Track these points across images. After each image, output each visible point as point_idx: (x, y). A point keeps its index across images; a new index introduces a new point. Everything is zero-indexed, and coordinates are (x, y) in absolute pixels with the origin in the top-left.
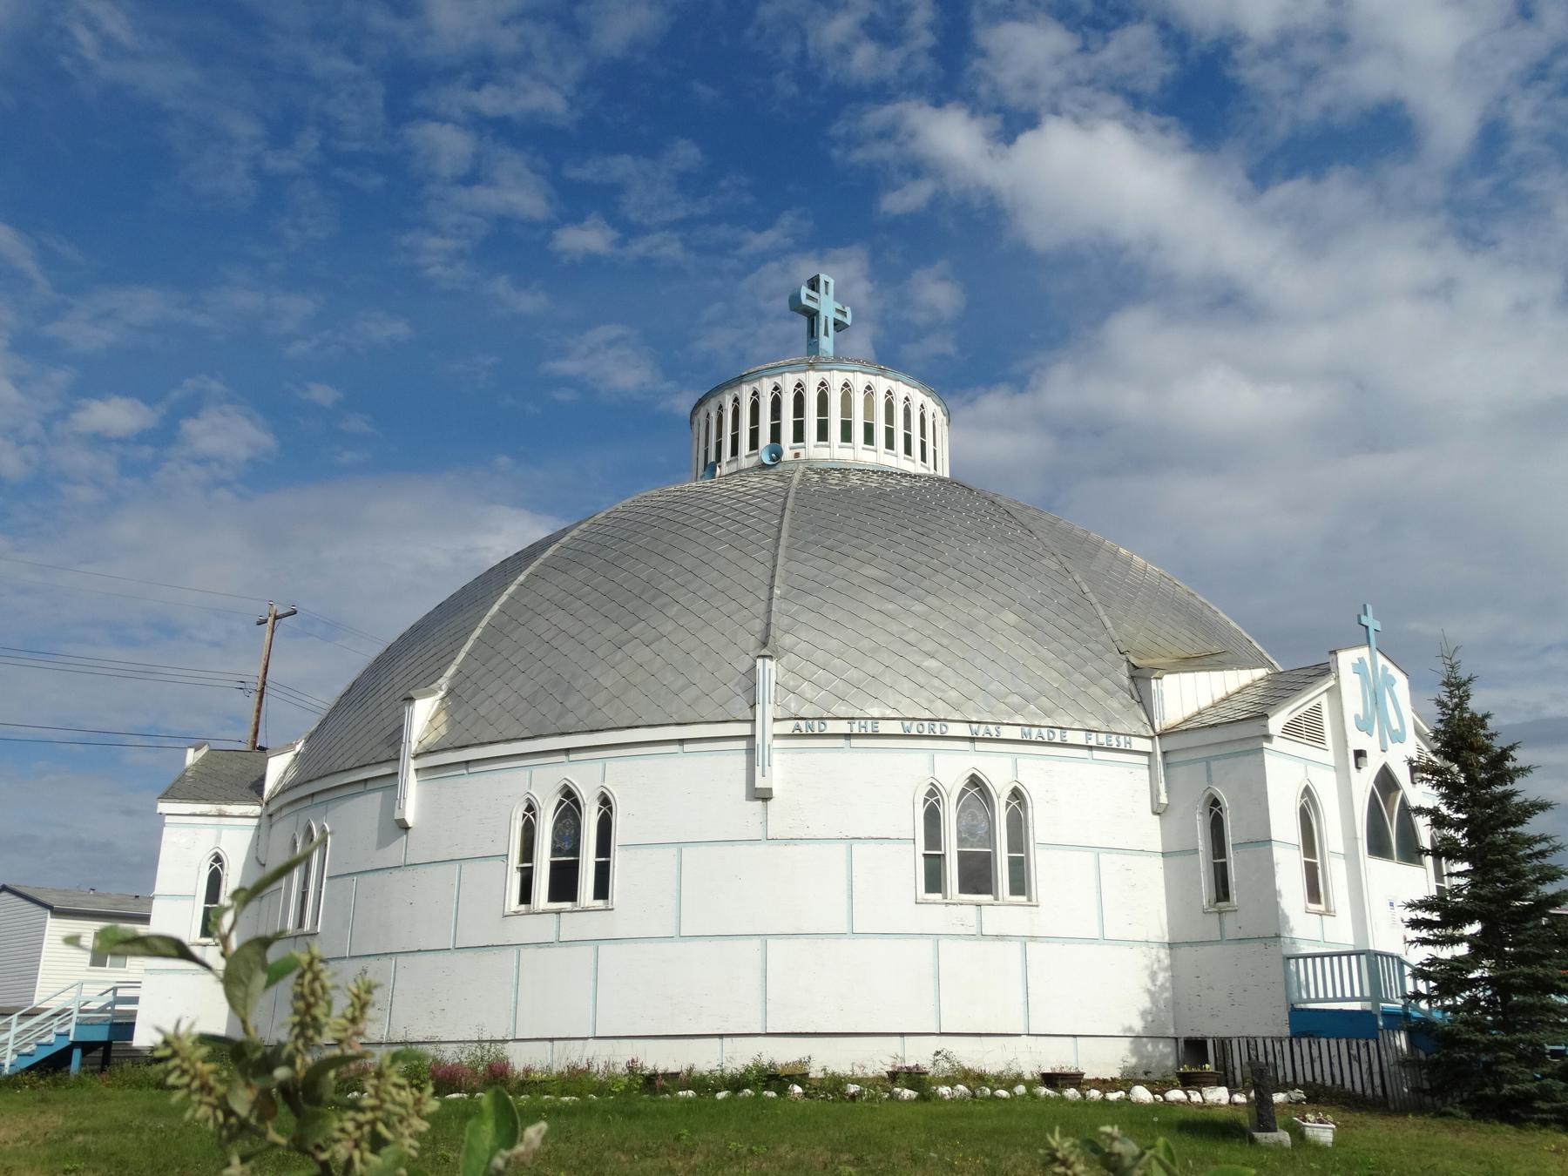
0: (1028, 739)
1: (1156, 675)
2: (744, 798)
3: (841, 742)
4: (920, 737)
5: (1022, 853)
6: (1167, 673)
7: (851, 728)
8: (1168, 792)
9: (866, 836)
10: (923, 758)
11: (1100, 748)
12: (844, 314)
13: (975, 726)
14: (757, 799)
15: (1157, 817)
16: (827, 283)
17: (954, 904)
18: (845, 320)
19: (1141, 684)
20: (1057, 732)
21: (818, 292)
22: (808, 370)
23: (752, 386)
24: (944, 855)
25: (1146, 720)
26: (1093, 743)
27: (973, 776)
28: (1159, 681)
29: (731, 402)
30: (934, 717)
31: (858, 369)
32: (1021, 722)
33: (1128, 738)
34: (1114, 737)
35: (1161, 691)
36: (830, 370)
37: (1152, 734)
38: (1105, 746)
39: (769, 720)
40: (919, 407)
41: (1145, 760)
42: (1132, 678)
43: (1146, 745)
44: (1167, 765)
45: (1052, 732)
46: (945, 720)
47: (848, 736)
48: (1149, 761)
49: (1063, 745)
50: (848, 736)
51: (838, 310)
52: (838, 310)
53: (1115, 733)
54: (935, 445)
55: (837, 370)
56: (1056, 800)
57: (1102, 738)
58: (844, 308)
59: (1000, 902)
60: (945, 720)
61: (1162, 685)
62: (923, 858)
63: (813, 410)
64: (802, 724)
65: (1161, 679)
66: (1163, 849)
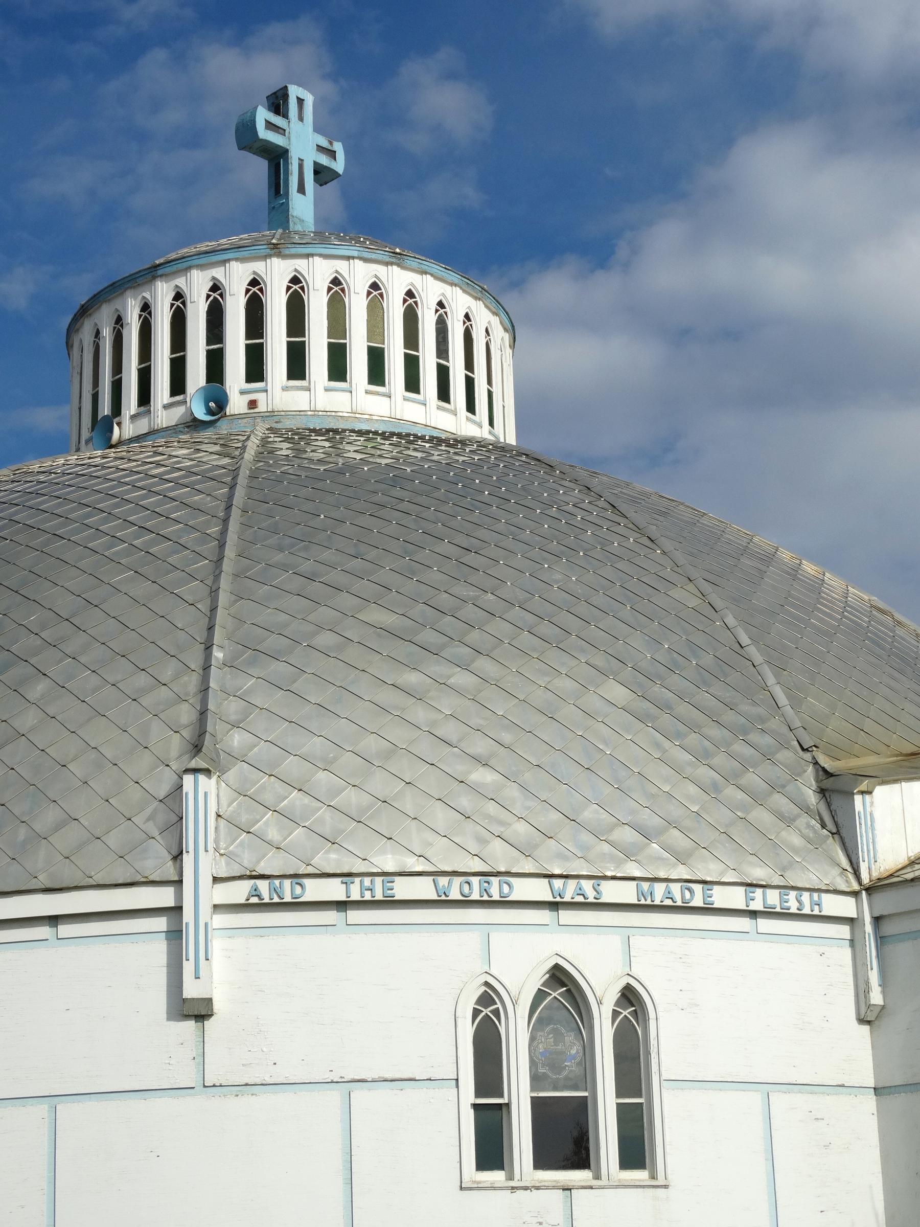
0: (649, 902)
3: (331, 916)
5: (640, 1096)
8: (883, 984)
9: (376, 1076)
10: (473, 938)
12: (332, 154)
13: (558, 883)
14: (187, 1017)
15: (866, 1029)
16: (300, 101)
17: (526, 1188)
19: (837, 801)
20: (697, 888)
24: (508, 1105)
28: (867, 797)
31: (355, 254)
32: (637, 873)
33: (815, 895)
34: (793, 894)
35: (871, 814)
36: (308, 256)
37: (856, 887)
38: (778, 910)
39: (205, 880)
41: (844, 931)
43: (845, 907)
44: (881, 940)
45: (689, 889)
46: (508, 874)
47: (342, 905)
48: (852, 932)
49: (708, 910)
50: (342, 905)
51: (320, 149)
52: (320, 149)
54: (490, 382)
55: (320, 255)
57: (773, 897)
58: (331, 143)
61: (872, 803)
62: (472, 1112)
63: (280, 323)
65: (870, 793)
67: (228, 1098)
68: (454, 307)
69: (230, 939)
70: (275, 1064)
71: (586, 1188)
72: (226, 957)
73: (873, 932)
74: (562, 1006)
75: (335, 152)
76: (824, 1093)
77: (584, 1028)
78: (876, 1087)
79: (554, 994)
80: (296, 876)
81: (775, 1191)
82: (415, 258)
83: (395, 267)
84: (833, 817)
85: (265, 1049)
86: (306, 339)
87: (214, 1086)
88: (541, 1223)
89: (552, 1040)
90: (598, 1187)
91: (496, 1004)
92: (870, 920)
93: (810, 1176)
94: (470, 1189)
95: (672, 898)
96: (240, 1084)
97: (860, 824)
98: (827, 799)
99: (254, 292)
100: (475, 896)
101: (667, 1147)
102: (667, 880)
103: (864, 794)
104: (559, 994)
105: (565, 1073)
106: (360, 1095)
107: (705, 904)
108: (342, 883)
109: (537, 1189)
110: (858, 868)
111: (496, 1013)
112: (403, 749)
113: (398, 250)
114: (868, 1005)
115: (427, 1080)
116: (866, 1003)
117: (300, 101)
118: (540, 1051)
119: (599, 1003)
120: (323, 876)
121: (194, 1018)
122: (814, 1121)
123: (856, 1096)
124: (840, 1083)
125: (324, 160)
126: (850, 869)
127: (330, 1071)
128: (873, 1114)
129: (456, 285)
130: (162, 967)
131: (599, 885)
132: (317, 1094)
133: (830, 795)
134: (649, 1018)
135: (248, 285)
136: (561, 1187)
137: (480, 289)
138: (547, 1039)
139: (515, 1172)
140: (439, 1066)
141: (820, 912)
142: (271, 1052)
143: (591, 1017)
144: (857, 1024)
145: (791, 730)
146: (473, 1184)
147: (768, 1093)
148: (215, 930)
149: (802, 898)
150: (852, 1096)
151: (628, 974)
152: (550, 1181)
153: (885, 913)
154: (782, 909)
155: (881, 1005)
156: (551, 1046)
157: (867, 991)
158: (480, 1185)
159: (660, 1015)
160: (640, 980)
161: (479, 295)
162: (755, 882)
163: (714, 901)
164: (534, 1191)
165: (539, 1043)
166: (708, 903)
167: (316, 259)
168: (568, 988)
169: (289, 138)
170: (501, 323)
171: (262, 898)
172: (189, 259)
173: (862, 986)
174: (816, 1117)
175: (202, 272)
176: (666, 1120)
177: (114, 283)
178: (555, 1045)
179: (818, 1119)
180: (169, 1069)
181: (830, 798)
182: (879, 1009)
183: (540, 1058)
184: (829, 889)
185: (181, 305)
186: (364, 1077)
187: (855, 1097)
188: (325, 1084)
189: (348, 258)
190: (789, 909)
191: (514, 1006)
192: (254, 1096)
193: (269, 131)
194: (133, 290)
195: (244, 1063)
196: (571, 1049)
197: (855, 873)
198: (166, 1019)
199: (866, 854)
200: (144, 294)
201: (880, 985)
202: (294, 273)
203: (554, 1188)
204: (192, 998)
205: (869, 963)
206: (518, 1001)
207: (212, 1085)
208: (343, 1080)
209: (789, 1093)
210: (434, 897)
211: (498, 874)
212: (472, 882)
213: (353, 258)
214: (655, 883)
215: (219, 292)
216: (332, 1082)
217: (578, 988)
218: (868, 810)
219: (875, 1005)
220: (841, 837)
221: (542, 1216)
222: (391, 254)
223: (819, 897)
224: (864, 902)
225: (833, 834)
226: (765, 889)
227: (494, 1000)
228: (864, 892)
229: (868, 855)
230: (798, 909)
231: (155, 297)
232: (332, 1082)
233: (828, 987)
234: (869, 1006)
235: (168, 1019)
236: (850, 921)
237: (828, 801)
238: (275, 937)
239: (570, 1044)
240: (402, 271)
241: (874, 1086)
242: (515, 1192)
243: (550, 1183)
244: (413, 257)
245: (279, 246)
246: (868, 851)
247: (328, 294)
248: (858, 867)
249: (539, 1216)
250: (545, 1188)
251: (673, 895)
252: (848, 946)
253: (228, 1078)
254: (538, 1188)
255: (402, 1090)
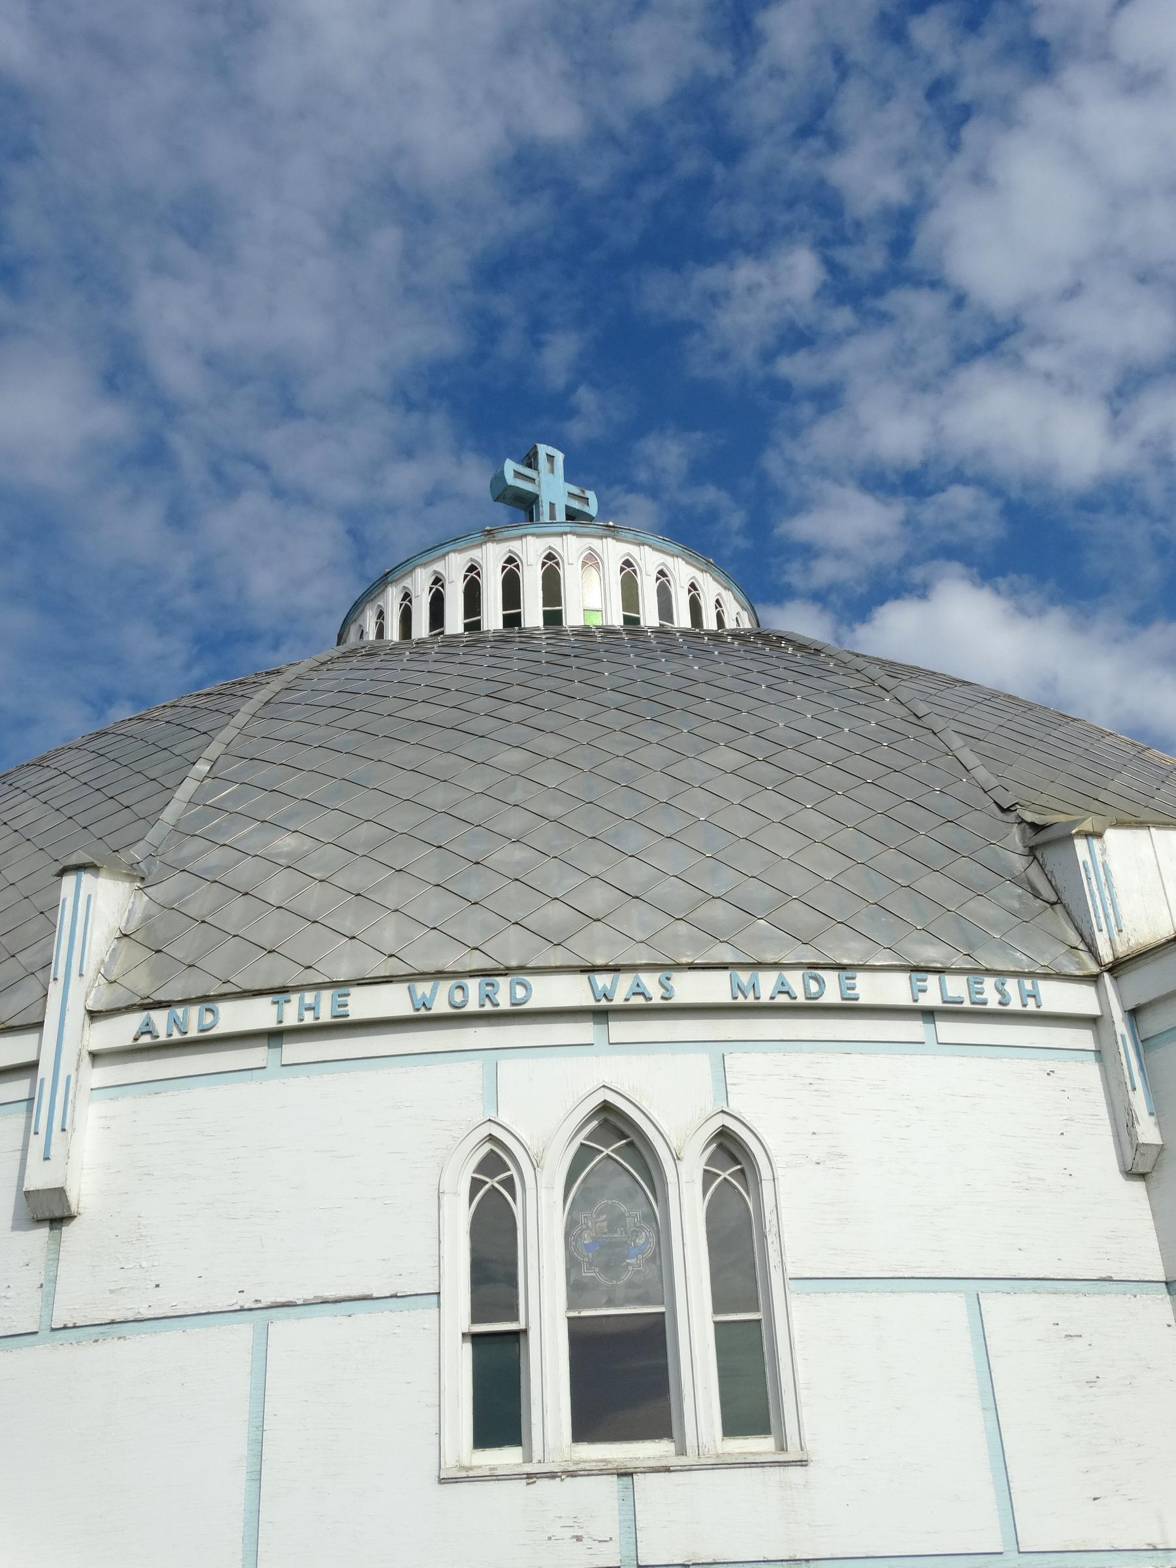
0: (751, 999)
1: (1087, 826)
2: (10, 1223)
3: (258, 1055)
4: (459, 1019)
5: (757, 1310)
6: (1119, 824)
7: (280, 1013)
8: (1156, 1111)
9: (309, 1295)
10: (469, 1072)
11: (953, 1012)
12: (585, 500)
13: (603, 980)
14: (39, 1221)
15: (1138, 1187)
16: (550, 458)
17: (552, 1475)
18: (586, 509)
19: (1051, 857)
20: (830, 977)
21: (536, 469)
22: (486, 542)
23: (401, 586)
24: (525, 1332)
25: (1074, 939)
26: (931, 998)
27: (606, 1108)
28: (1095, 842)
29: (374, 619)
30: (488, 964)
31: (568, 529)
32: (729, 958)
33: (1028, 984)
34: (989, 983)
35: (1104, 864)
36: (521, 537)
37: (1094, 969)
38: (967, 1004)
39: (76, 1015)
40: (687, 587)
41: (1084, 1038)
42: (1032, 851)
43: (1081, 1000)
44: (1144, 1044)
45: (816, 979)
46: (522, 969)
47: (275, 1036)
48: (1098, 1038)
49: (850, 1010)
50: (275, 1036)
51: (571, 495)
52: (571, 495)
53: (989, 972)
55: (533, 535)
56: (841, 1156)
57: (957, 987)
58: (583, 492)
59: (690, 1459)
60: (522, 969)
61: (1104, 851)
62: (468, 1347)
63: (496, 598)
64: (160, 1018)
65: (1099, 835)
66: (1167, 1271)
67: (82, 1345)
68: (676, 575)
69: (112, 1101)
70: (157, 1286)
71: (659, 1472)
72: (103, 1128)
73: (1128, 1032)
74: (621, 1169)
75: (588, 499)
76: (1078, 1292)
77: (657, 1202)
78: (1170, 1280)
79: (606, 1151)
80: (204, 999)
81: (1005, 1464)
82: (630, 530)
83: (609, 540)
84: (1050, 882)
85: (144, 1264)
86: (522, 610)
87: (65, 1328)
88: (579, 1539)
89: (605, 1224)
90: (679, 1468)
91: (509, 1170)
92: (1121, 1016)
93: (1068, 1436)
94: (455, 1480)
95: (788, 993)
96: (103, 1322)
97: (1088, 879)
98: (1038, 861)
99: (472, 577)
100: (472, 1006)
101: (802, 1393)
102: (776, 966)
103: (1090, 838)
104: (614, 1151)
105: (626, 1277)
106: (283, 1328)
107: (843, 999)
108: (274, 1003)
109: (572, 1476)
110: (1092, 941)
111: (509, 1183)
112: (403, 833)
113: (611, 524)
114: (1135, 1145)
115: (391, 1297)
116: (1131, 1143)
117: (550, 458)
118: (585, 1242)
119: (676, 1158)
120: (244, 997)
121: (48, 1223)
122: (1066, 1339)
123: (1135, 1296)
124: (1104, 1275)
125: (576, 505)
126: (1081, 946)
127: (240, 1292)
128: (1169, 1326)
129: (677, 557)
130: (15, 1151)
131: (668, 979)
132: (217, 1330)
133: (1042, 854)
134: (761, 1180)
135: (466, 572)
136: (615, 1471)
137: (706, 562)
138: (596, 1223)
139: (534, 1448)
140: (411, 1273)
141: (1039, 1007)
142: (153, 1268)
143: (664, 1183)
144: (1124, 1181)
145: (985, 792)
146: (459, 1471)
147: (978, 1295)
148: (94, 1091)
149: (1006, 987)
150: (1129, 1295)
151: (723, 1112)
152: (594, 1461)
153: (1143, 1001)
154: (973, 1003)
155: (1157, 1145)
156: (605, 1233)
157: (1130, 1124)
158: (471, 1473)
159: (779, 1173)
160: (742, 1119)
161: (704, 567)
162: (922, 964)
163: (858, 994)
164: (569, 1480)
165: (582, 1230)
166: (848, 997)
167: (530, 538)
168: (628, 1140)
169: (539, 486)
170: (735, 598)
171: (155, 1034)
172: (414, 559)
173: (1123, 1118)
174: (1067, 1334)
175: (426, 569)
176: (797, 1346)
177: (356, 602)
178: (610, 1232)
179: (1071, 1336)
180: (5, 1306)
181: (1042, 857)
182: (1155, 1152)
183: (585, 1254)
184: (1049, 972)
185: (408, 603)
186: (291, 1299)
187: (1132, 1297)
188: (231, 1314)
189: (561, 534)
190: (985, 1004)
191: (535, 1169)
192: (122, 1340)
193: (518, 480)
194: (371, 603)
195: (112, 1288)
196: (637, 1236)
197: (1090, 951)
198: (10, 1229)
199: (1102, 920)
200: (379, 603)
201: (1151, 1114)
202: (509, 554)
203: (602, 1472)
204: (36, 1190)
205: (1128, 1081)
206: (542, 1161)
207: (62, 1326)
208: (259, 1305)
209: (1015, 1293)
210: (408, 1011)
211: (506, 971)
212: (468, 988)
213: (566, 533)
214: (760, 973)
215: (439, 584)
216: (242, 1310)
217: (644, 1138)
218: (1099, 859)
219: (1146, 1144)
220: (1064, 906)
221: (581, 1525)
222: (604, 528)
223: (1034, 986)
224: (1107, 986)
225: (1052, 904)
226: (942, 975)
227: (505, 1164)
228: (1106, 975)
229: (1107, 923)
230: (1000, 1003)
231: (386, 603)
232: (242, 1310)
233: (1066, 1122)
234: (1137, 1147)
235: (14, 1228)
236: (1092, 1021)
237: (1041, 862)
238: (176, 1093)
239: (636, 1229)
240: (618, 543)
241: (1164, 1279)
242: (535, 1482)
243: (594, 1464)
244: (627, 529)
245: (492, 532)
246: (1106, 916)
247: (542, 568)
248: (1093, 939)
249: (575, 1524)
250: (586, 1473)
251: (790, 987)
252: (1094, 1061)
253: (86, 1314)
254: (572, 1474)
255: (349, 1316)
